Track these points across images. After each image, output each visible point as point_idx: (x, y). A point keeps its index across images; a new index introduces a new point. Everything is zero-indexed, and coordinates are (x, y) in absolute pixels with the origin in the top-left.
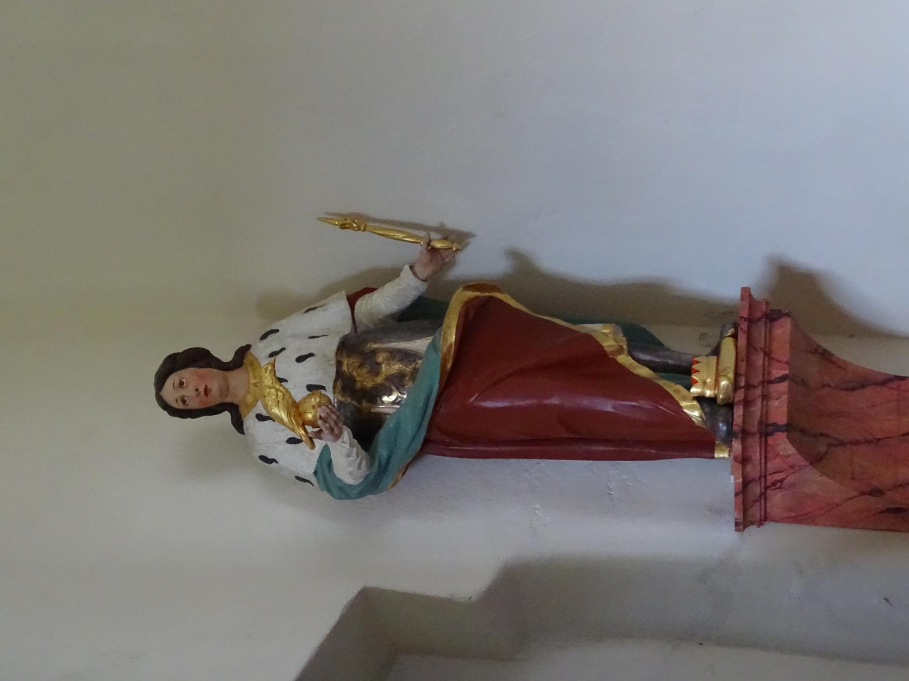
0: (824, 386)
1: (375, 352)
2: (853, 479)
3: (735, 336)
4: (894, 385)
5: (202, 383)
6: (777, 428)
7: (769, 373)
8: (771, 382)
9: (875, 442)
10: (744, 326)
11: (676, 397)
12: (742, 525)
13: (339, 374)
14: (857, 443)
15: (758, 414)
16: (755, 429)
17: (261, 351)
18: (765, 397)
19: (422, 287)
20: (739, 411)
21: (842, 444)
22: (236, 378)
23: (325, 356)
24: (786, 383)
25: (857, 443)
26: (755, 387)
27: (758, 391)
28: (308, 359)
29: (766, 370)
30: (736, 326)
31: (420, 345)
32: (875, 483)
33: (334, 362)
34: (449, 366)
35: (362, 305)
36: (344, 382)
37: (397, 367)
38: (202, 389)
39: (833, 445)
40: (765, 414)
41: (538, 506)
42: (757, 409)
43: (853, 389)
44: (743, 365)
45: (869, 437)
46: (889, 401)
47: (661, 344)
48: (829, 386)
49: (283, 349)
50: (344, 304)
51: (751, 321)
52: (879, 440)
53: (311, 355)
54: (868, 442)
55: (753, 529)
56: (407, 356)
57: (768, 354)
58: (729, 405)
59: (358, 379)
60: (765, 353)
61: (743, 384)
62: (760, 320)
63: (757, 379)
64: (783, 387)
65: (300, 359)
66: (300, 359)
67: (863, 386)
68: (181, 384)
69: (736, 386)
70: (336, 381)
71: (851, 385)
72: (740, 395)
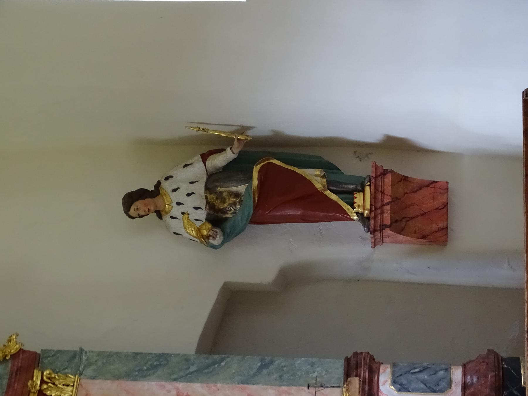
0: (405, 194)
1: (221, 193)
2: (415, 233)
3: (370, 185)
4: (432, 186)
5: (141, 201)
6: (387, 226)
7: (383, 201)
8: (384, 205)
9: (424, 214)
10: (373, 181)
11: (348, 213)
12: (375, 244)
13: (207, 202)
14: (417, 216)
15: (379, 222)
16: (378, 228)
17: (167, 186)
18: (382, 213)
19: (235, 156)
20: (372, 222)
21: (412, 218)
22: (158, 199)
23: (200, 195)
24: (389, 206)
25: (417, 216)
26: (378, 209)
27: (379, 211)
28: (192, 195)
29: (382, 200)
30: (370, 181)
31: (241, 189)
32: (424, 233)
33: (204, 197)
34: (257, 200)
35: (209, 163)
36: (210, 205)
37: (232, 200)
38: (147, 210)
39: (408, 221)
40: (382, 220)
41: (291, 240)
42: (379, 219)
43: (416, 191)
44: (373, 200)
45: (422, 213)
46: (430, 194)
47: (339, 170)
48: (407, 193)
49: (178, 188)
50: (202, 164)
51: (376, 177)
52: (426, 213)
53: (193, 193)
54: (421, 215)
55: (378, 246)
56: (237, 195)
57: (383, 193)
58: (368, 218)
59: (216, 205)
60: (382, 192)
61: (373, 209)
62: (379, 176)
63: (379, 205)
64: (388, 207)
65: (189, 195)
66: (189, 195)
67: (420, 188)
68: (137, 208)
69: (371, 211)
70: (206, 205)
71: (415, 189)
72: (372, 215)
